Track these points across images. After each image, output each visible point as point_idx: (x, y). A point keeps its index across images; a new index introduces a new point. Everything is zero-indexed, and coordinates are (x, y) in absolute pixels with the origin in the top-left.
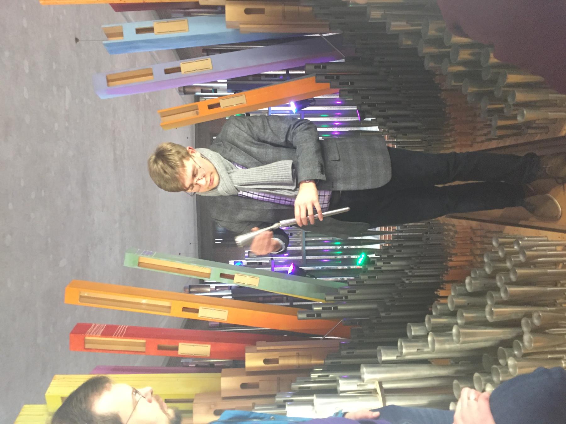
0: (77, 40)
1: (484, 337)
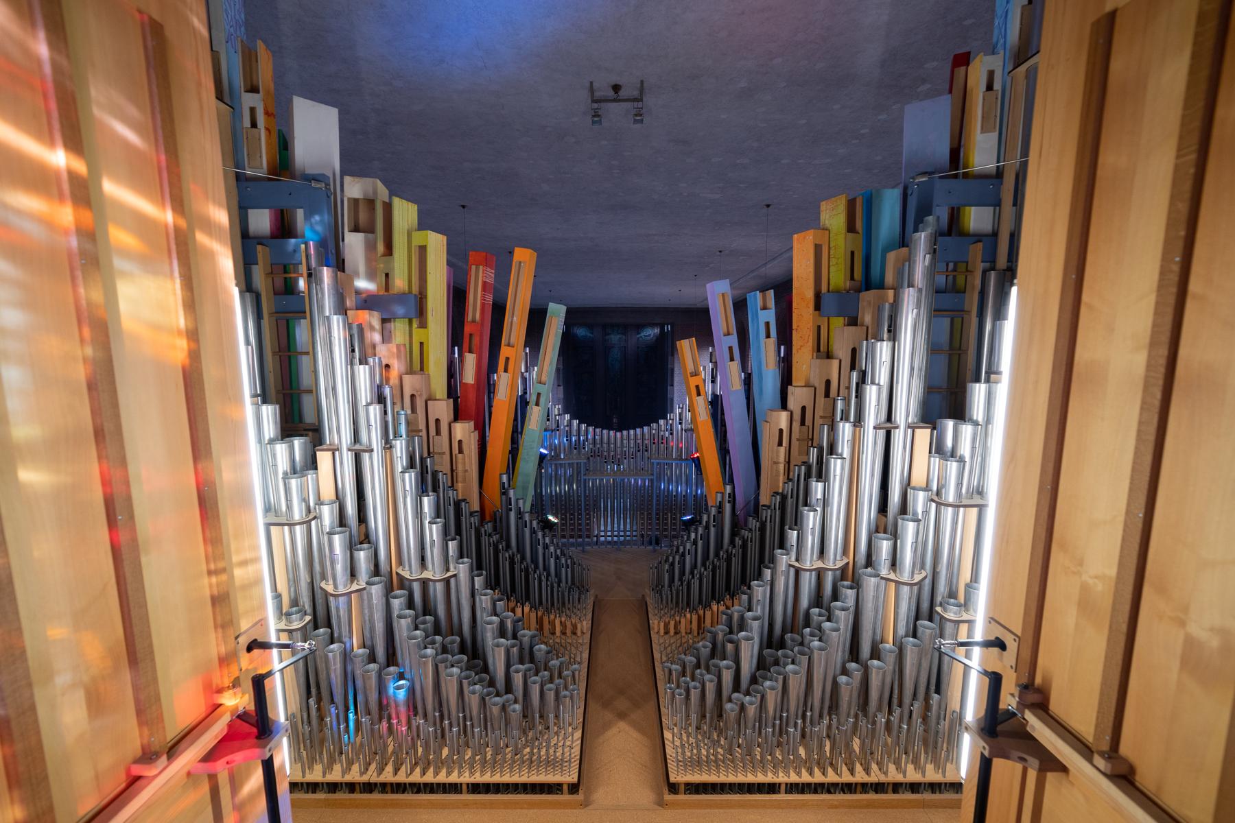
0: (768, 206)
1: (497, 662)
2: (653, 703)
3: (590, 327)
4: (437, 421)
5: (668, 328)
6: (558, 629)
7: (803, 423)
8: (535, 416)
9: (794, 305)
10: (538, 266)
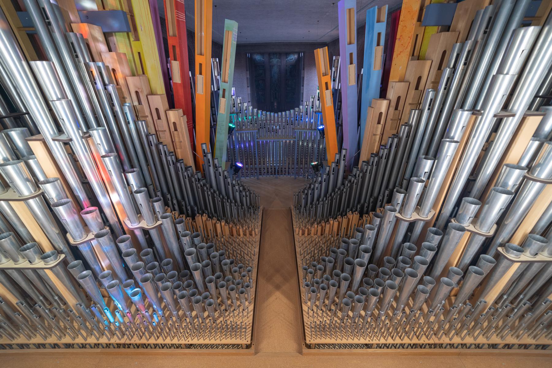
2: (295, 278)
3: (262, 54)
4: (157, 110)
5: (302, 55)
6: (241, 233)
7: (396, 108)
8: (223, 104)
9: (401, 18)
10: (239, 28)
